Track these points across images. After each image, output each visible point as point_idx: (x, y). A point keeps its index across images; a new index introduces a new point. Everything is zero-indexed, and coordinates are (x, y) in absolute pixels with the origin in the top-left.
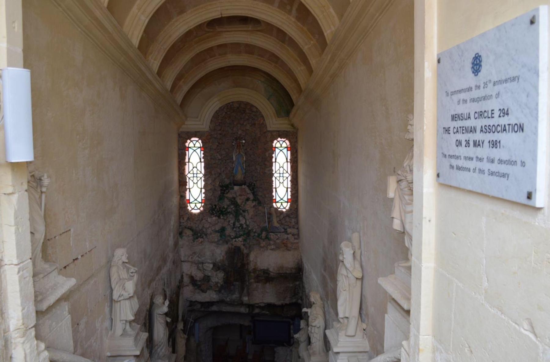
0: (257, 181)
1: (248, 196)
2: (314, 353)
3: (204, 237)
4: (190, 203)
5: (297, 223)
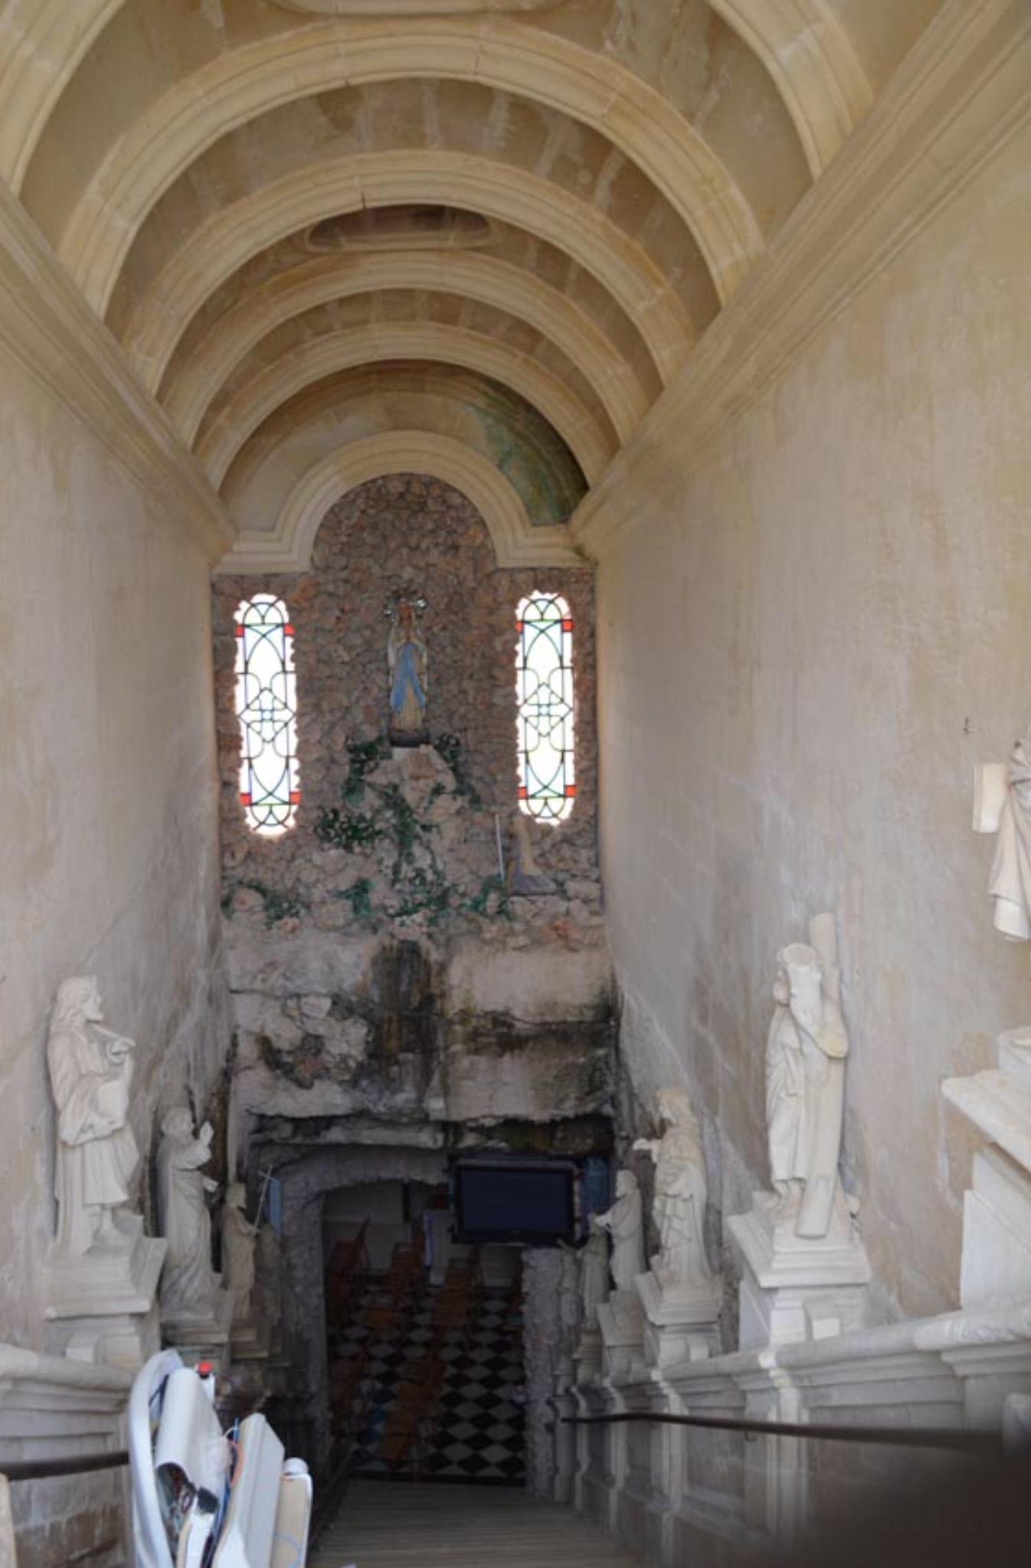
0: (466, 729)
1: (441, 778)
2: (673, 1280)
3: (303, 912)
4: (251, 805)
5: (597, 862)
